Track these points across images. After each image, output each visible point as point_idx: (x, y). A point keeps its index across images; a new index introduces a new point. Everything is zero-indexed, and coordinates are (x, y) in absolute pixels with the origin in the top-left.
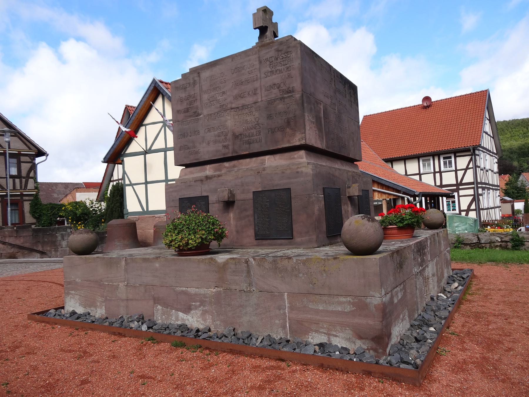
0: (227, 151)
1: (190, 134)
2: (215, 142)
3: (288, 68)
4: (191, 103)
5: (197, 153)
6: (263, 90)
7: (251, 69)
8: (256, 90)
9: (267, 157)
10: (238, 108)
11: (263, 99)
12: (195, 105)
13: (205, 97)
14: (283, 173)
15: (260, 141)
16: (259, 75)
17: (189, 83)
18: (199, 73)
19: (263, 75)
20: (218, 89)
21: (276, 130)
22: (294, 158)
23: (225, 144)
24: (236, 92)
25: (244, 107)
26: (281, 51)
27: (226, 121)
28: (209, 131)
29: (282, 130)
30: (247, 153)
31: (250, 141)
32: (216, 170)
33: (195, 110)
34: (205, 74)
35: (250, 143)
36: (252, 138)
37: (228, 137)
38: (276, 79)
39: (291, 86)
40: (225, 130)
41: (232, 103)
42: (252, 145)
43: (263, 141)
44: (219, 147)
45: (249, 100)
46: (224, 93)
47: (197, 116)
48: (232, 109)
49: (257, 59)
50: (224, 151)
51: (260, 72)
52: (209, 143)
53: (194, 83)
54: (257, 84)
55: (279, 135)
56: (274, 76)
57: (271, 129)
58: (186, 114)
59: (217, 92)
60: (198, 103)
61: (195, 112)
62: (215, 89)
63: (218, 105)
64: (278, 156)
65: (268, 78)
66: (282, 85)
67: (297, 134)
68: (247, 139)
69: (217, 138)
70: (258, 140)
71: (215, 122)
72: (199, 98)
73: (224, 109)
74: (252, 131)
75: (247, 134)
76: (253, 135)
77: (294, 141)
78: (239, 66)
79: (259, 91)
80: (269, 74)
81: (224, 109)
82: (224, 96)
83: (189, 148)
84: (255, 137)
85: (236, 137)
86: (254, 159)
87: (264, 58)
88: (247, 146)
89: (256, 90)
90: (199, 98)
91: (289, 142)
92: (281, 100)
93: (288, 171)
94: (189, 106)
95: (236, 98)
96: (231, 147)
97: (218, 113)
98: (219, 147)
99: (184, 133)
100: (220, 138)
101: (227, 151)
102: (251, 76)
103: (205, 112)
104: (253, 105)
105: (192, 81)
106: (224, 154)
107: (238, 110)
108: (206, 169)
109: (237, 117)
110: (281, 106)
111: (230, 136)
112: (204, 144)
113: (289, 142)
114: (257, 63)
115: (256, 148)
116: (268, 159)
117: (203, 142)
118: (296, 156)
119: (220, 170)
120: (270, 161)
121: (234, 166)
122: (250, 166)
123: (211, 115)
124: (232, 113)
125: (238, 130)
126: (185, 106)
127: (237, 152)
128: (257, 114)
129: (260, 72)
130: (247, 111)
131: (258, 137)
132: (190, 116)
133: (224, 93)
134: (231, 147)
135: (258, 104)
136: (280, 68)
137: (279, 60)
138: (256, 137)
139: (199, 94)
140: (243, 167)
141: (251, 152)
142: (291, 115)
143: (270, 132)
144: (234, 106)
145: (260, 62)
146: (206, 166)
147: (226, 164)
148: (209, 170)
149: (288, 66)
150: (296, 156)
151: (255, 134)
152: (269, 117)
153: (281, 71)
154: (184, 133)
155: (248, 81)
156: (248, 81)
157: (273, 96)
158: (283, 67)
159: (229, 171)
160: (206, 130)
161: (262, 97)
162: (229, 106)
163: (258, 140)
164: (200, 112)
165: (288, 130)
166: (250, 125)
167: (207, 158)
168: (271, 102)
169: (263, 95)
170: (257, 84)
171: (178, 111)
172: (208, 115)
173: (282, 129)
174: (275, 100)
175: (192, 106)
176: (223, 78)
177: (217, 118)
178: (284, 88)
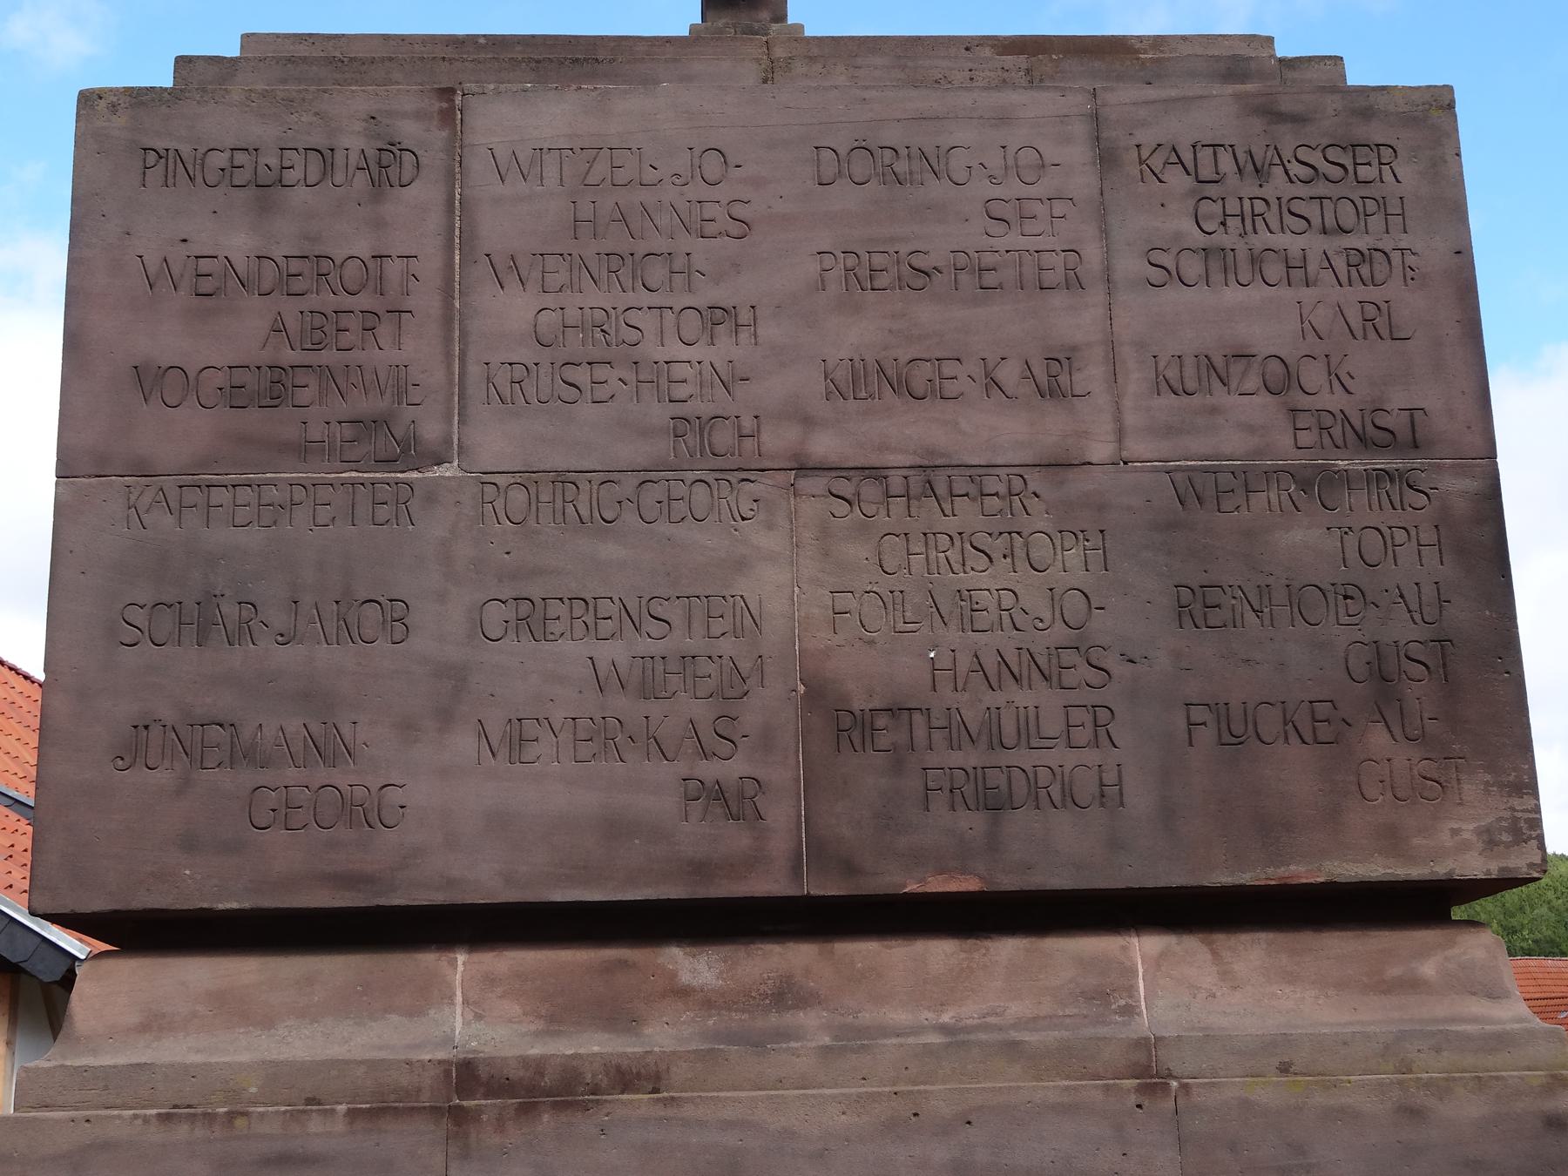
0: (737, 839)
1: (279, 619)
2: (604, 738)
3: (1361, 258)
4: (322, 330)
5: (364, 814)
6: (1136, 379)
7: (1014, 188)
8: (1062, 359)
9: (1141, 949)
10: (875, 473)
11: (1137, 447)
12: (381, 356)
13: (507, 312)
14: (1413, 1113)
15: (1109, 796)
16: (1093, 254)
17: (326, 155)
18: (447, 93)
19: (1130, 265)
20: (656, 273)
21: (1270, 723)
22: (1413, 985)
23: (710, 770)
24: (857, 335)
25: (931, 478)
26: (1298, 119)
27: (740, 565)
28: (531, 619)
29: (1325, 731)
30: (970, 885)
31: (997, 779)
32: (560, 1012)
33: (364, 405)
34: (504, 120)
35: (995, 804)
36: (1023, 758)
37: (751, 716)
38: (1262, 317)
39: (1398, 399)
40: (726, 646)
41: (808, 422)
42: (1020, 823)
43: (1140, 798)
44: (652, 790)
45: (998, 432)
46: (718, 317)
47: (388, 462)
48: (804, 468)
49: (1080, 129)
50: (700, 834)
51: (1105, 233)
52: (517, 742)
53: (386, 166)
54: (1076, 322)
55: (1293, 772)
56: (1232, 295)
57: (1220, 710)
58: (253, 420)
59: (646, 298)
60: (416, 349)
61: (380, 423)
62: (625, 265)
63: (659, 413)
64: (1251, 951)
65: (1174, 296)
66: (1313, 375)
67: (1471, 789)
68: (970, 758)
69: (623, 705)
70: (1086, 788)
71: (610, 550)
72: (425, 300)
73: (711, 453)
74: (1023, 698)
75: (972, 717)
76: (1029, 733)
77: (1445, 839)
78: (892, 136)
79: (1091, 376)
80: (1192, 268)
81: (711, 453)
82: (724, 350)
83: (244, 754)
84: (1053, 757)
85: (842, 722)
86: (1007, 949)
87: (1147, 137)
88: (972, 823)
89: (1062, 359)
90: (425, 300)
91: (1391, 840)
92: (1305, 486)
93: (1469, 1108)
94: (289, 356)
95: (863, 381)
96: (781, 815)
97: (646, 475)
98: (652, 790)
99: (209, 600)
100: (655, 708)
101: (737, 839)
102: (1013, 240)
103: (497, 441)
104: (1035, 481)
105: (353, 141)
106: (699, 869)
107: (871, 491)
108: (431, 994)
109: (858, 552)
110: (1303, 540)
111: (772, 703)
112: (464, 743)
113: (1391, 840)
114: (1077, 154)
115: (1061, 853)
116: (1157, 963)
117: (445, 717)
118: (1428, 969)
119: (618, 1017)
120: (1172, 986)
121: (785, 995)
122: (968, 1011)
123: (562, 478)
124: (812, 509)
125: (870, 668)
126: (244, 335)
127: (850, 868)
128: (1071, 564)
129: (1105, 233)
130: (967, 515)
131: (1092, 756)
132: (303, 450)
133: (718, 317)
134: (781, 815)
135: (1080, 484)
136: (1292, 244)
137: (1277, 185)
138: (1060, 757)
139: (430, 265)
140: (899, 1016)
141: (1009, 882)
142: (1402, 630)
143: (1206, 735)
144: (824, 446)
145: (1106, 159)
146: (428, 959)
147: (696, 966)
148: (472, 1008)
149: (1362, 242)
150: (1428, 969)
151: (1052, 726)
152: (1196, 606)
153: (1295, 268)
154: (209, 600)
155: (980, 276)
156: (980, 276)
157: (1231, 443)
158: (1315, 244)
159: (757, 1043)
160: (496, 615)
161: (1120, 430)
162: (778, 440)
163: (1086, 788)
164: (431, 431)
165: (1379, 739)
166: (1006, 641)
167: (485, 879)
168: (1201, 491)
169: (1130, 419)
170: (1076, 322)
171: (148, 379)
172: (528, 478)
173: (1322, 727)
174: (1248, 480)
175: (328, 357)
176: (723, 193)
177: (630, 518)
178: (1333, 400)
